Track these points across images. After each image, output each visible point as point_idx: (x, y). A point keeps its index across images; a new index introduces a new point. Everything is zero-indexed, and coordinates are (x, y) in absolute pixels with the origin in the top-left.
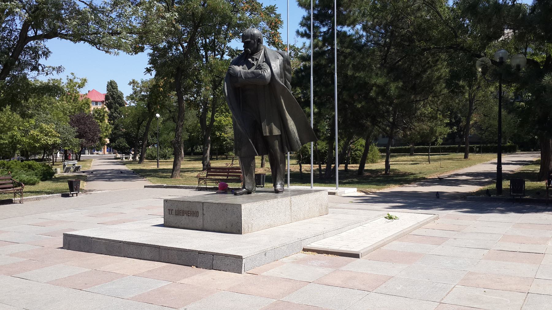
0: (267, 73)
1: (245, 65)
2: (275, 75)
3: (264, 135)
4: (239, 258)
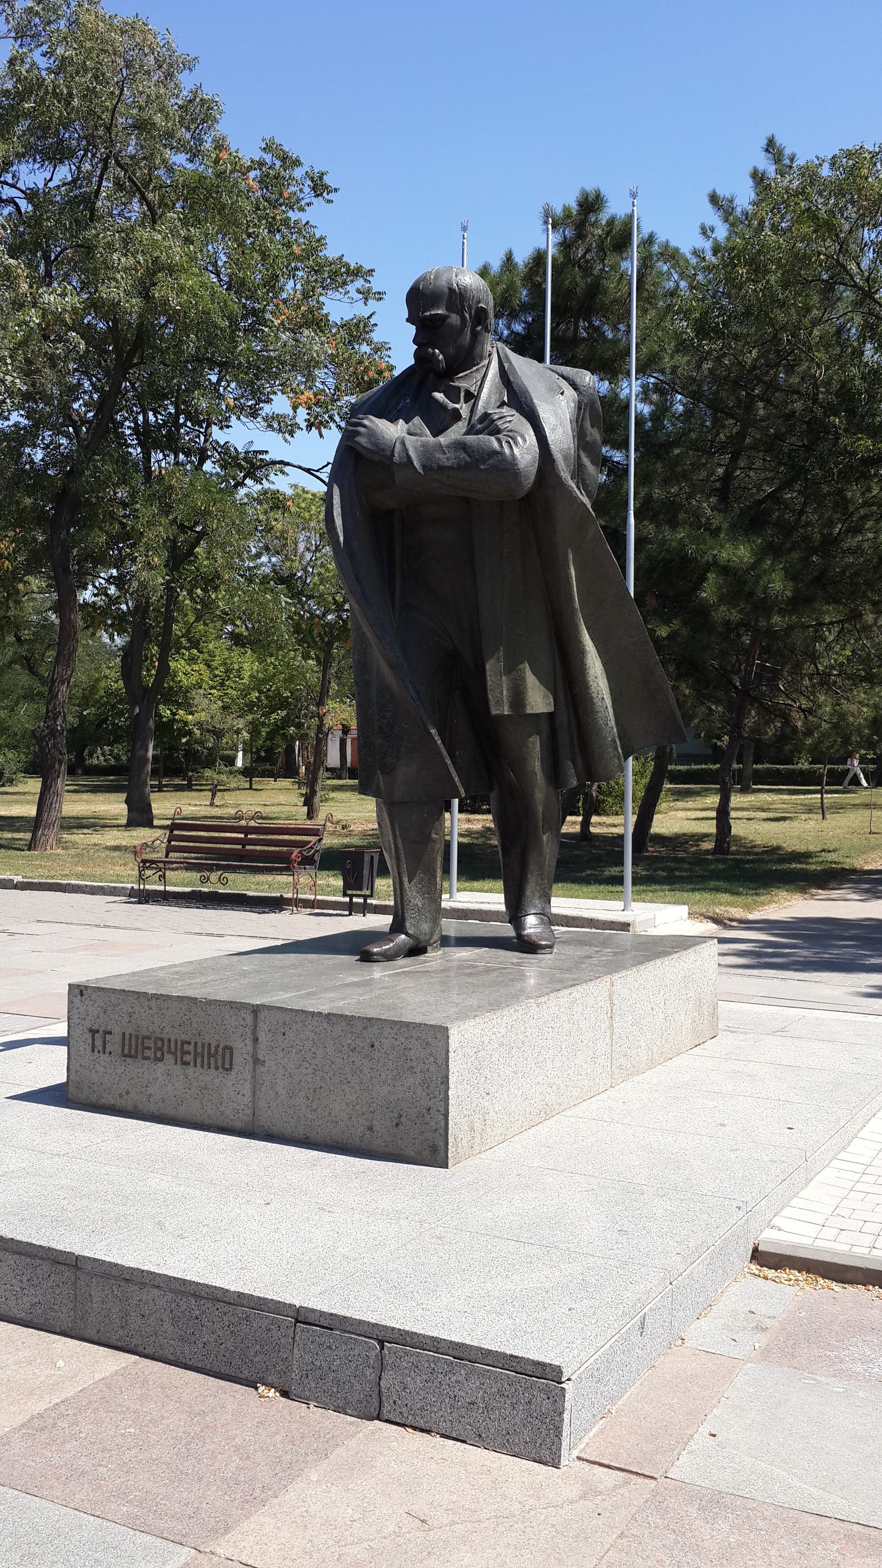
0: (524, 451)
1: (417, 420)
2: (558, 456)
3: (494, 712)
4: (542, 1379)
